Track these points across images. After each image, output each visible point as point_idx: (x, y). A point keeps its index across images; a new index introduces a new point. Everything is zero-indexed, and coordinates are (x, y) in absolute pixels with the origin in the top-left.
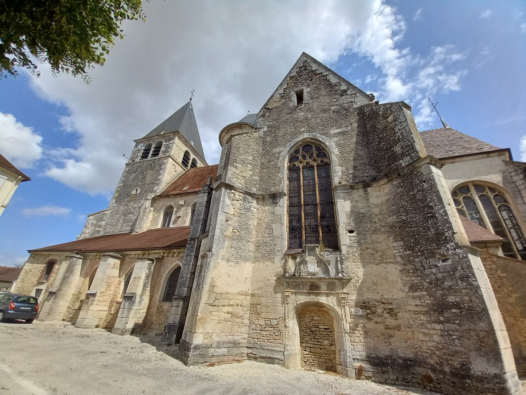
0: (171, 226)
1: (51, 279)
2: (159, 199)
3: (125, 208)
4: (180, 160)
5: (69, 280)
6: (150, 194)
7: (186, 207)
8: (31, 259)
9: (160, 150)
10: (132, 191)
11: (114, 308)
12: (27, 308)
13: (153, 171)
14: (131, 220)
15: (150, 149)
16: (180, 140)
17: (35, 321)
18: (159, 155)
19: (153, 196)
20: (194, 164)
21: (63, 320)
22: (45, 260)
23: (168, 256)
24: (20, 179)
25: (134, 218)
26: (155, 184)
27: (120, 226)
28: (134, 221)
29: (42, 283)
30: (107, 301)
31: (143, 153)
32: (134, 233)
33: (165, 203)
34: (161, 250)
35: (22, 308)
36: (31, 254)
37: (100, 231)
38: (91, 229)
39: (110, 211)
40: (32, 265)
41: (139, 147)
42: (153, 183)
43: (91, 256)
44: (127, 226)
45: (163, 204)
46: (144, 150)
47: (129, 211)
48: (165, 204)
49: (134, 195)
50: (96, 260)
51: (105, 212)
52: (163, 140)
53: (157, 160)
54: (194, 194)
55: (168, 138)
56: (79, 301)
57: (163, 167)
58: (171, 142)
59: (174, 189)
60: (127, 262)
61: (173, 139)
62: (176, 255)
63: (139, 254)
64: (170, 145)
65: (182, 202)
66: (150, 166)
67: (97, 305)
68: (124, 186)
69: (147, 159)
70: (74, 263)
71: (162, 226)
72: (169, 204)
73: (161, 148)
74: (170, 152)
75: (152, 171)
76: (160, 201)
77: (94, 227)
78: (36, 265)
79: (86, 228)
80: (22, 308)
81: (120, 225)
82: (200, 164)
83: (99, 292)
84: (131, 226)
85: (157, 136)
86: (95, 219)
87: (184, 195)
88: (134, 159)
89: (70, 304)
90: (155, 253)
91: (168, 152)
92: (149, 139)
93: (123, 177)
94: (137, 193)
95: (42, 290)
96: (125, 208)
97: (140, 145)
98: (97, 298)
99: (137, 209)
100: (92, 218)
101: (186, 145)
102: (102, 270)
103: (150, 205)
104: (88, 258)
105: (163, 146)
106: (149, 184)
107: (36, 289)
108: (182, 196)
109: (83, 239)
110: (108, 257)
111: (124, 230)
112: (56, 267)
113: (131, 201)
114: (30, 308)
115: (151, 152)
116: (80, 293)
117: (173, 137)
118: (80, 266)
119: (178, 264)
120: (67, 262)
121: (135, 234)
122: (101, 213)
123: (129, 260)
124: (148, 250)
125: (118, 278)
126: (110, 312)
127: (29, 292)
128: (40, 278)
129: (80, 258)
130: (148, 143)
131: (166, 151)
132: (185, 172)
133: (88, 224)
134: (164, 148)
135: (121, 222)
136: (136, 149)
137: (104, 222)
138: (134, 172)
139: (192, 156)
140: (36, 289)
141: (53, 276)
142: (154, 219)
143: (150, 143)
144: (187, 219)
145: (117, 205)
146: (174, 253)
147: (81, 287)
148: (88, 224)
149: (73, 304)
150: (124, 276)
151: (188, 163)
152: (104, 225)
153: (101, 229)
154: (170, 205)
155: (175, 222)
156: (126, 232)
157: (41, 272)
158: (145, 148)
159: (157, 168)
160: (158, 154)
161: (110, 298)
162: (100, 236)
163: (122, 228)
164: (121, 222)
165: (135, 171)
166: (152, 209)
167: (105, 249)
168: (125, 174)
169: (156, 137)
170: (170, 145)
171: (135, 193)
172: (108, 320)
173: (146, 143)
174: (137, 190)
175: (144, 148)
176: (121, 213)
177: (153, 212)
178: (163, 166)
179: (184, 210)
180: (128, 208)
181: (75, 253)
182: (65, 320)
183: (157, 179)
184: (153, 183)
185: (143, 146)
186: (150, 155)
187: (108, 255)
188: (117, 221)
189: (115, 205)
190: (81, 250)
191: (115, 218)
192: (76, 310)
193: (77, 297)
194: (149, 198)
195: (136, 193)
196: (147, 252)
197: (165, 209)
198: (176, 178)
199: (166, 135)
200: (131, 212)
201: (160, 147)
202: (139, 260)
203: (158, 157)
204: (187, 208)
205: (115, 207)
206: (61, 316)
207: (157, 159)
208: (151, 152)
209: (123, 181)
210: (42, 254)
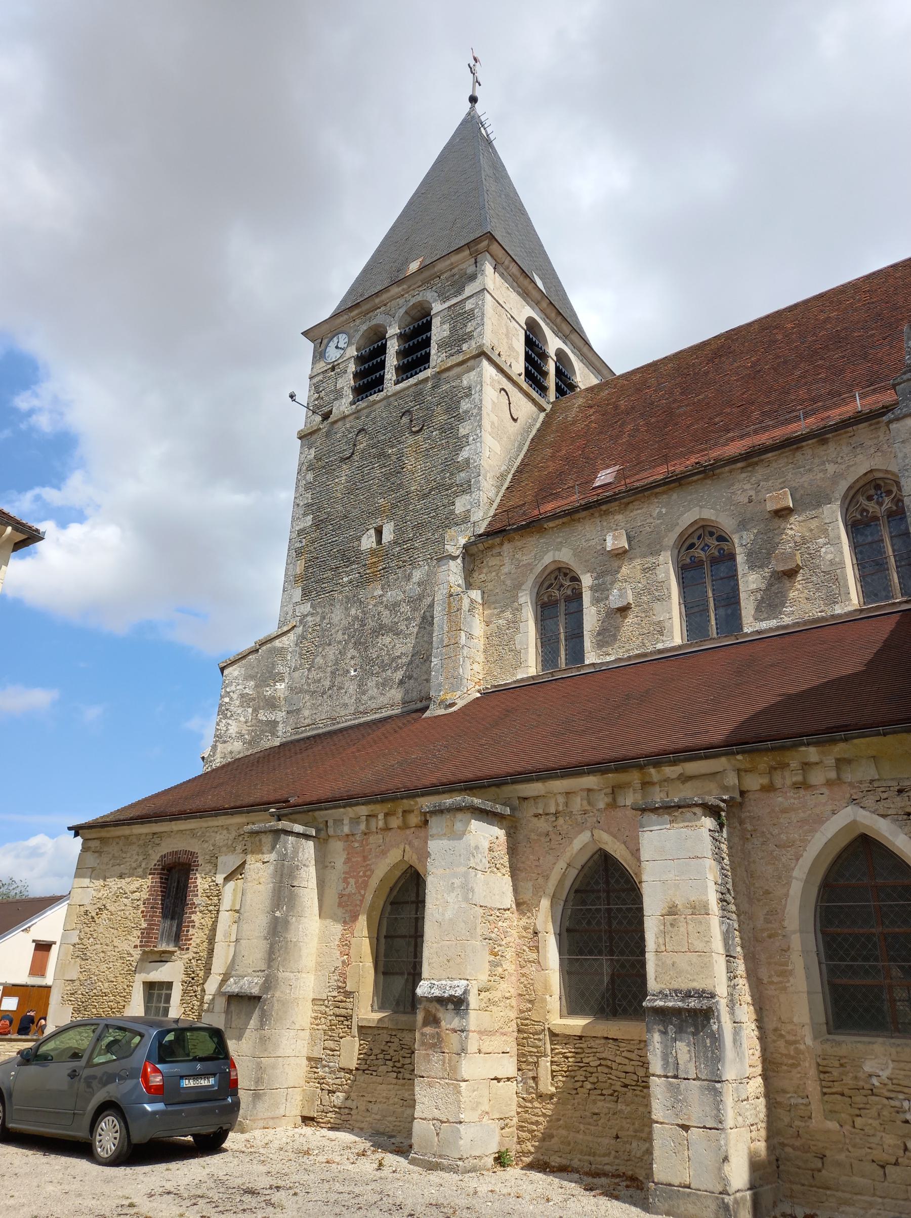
0: (591, 657)
1: (197, 937)
2: (490, 548)
3: (353, 612)
4: (518, 366)
5: (291, 936)
6: (451, 532)
7: (644, 556)
8: (91, 860)
9: (429, 340)
10: (359, 539)
11: (545, 1064)
12: (204, 1082)
13: (425, 433)
14: (394, 660)
15: (382, 350)
16: (502, 275)
17: (233, 1140)
18: (432, 363)
19: (462, 541)
20: (565, 384)
21: (307, 1120)
22: (147, 856)
23: (769, 788)
24: (9, 538)
25: (404, 647)
26: (451, 486)
27: (351, 691)
28: (405, 660)
29: (163, 958)
30: (506, 1029)
31: (356, 375)
32: (434, 711)
33: (526, 559)
34: (723, 760)
35: (186, 1083)
36: (86, 840)
37: (274, 723)
38: (242, 719)
39: (292, 636)
40: (101, 882)
41: (333, 354)
42: (442, 487)
43: (346, 821)
44: (384, 685)
45: (517, 567)
46: (360, 360)
47: (371, 624)
48: (530, 567)
49: (373, 552)
50: (372, 839)
51: (277, 643)
52: (430, 295)
53: (430, 384)
54: (664, 493)
55: (447, 279)
56: (355, 1031)
57: (465, 405)
58: (469, 290)
59: (545, 492)
60: (533, 836)
61: (473, 277)
62: (817, 777)
63: (589, 790)
64: (469, 305)
65: (614, 541)
66: (405, 420)
67: (480, 1052)
68: (318, 524)
69: (381, 395)
70: (293, 858)
71: (540, 667)
72: (548, 559)
73: (430, 330)
74: (481, 334)
75: (419, 437)
76: (499, 554)
77: (250, 710)
78: (114, 884)
79: (226, 717)
80: (186, 1083)
81: (352, 688)
82: (584, 378)
83: (473, 992)
84: (401, 682)
85: (398, 283)
86: (248, 677)
87: (614, 506)
88: (326, 409)
89: (313, 1041)
90: (685, 779)
91: (469, 336)
92: (365, 307)
93: (301, 489)
94: (384, 541)
95: (169, 985)
96: (353, 612)
97: (332, 345)
98: (475, 1019)
99: (405, 608)
100: (236, 673)
101: (525, 294)
102: (457, 882)
103: (461, 581)
104: (331, 831)
105: (436, 322)
106: (425, 496)
107: (145, 983)
108: (607, 513)
109: (224, 762)
110: (460, 816)
111: (373, 705)
112: (201, 883)
113: (369, 581)
114: (212, 1081)
115: (391, 360)
116: (348, 994)
117: (471, 270)
118: (312, 870)
119: (854, 823)
120: (266, 857)
121: (442, 712)
122: (264, 648)
123: (542, 825)
124: (641, 767)
125: (516, 915)
126: (531, 1083)
127: (119, 999)
128: (146, 935)
129: (307, 837)
130: (364, 327)
131: (457, 340)
132: (542, 415)
133: (227, 700)
134: (446, 326)
135: (353, 673)
136: (322, 364)
137: (283, 686)
138: (343, 460)
139: (553, 344)
140: (145, 983)
141: (197, 924)
142: (496, 640)
143: (374, 322)
144: (670, 612)
145: (312, 606)
146: (806, 766)
147: (340, 964)
148: (227, 700)
149: (331, 1044)
150: (545, 903)
151: (545, 374)
152: (285, 699)
153: (280, 715)
154: (552, 567)
155: (606, 636)
156: (385, 713)
157: (142, 908)
158: (358, 350)
159: (442, 418)
160: (425, 360)
161: (513, 1015)
162: (283, 745)
163: (365, 698)
164: (353, 673)
165: (347, 454)
166: (476, 595)
167: (690, 747)
168: (310, 476)
169: (395, 290)
170: (469, 305)
171: (374, 545)
172: (537, 1123)
173: (357, 331)
174: (379, 532)
175: (352, 352)
176: (340, 637)
177: (481, 608)
178: (463, 403)
179: (639, 575)
180: (364, 613)
181: (272, 815)
182: (312, 1119)
183: (452, 466)
184: (442, 487)
185: (349, 344)
186: (390, 374)
187: (460, 809)
188: (333, 673)
189: (307, 608)
190: (287, 801)
191: (319, 660)
192: (350, 1071)
193: (337, 1011)
194: (451, 549)
195: (379, 541)
196: (634, 777)
197: (533, 586)
198: (520, 449)
199: (441, 266)
200: (382, 626)
201: (428, 327)
202: (654, 817)
203: (428, 373)
204: (651, 559)
205: (309, 618)
206: (294, 1107)
207: (426, 380)
208: (391, 360)
209: (307, 505)
210: (127, 837)
